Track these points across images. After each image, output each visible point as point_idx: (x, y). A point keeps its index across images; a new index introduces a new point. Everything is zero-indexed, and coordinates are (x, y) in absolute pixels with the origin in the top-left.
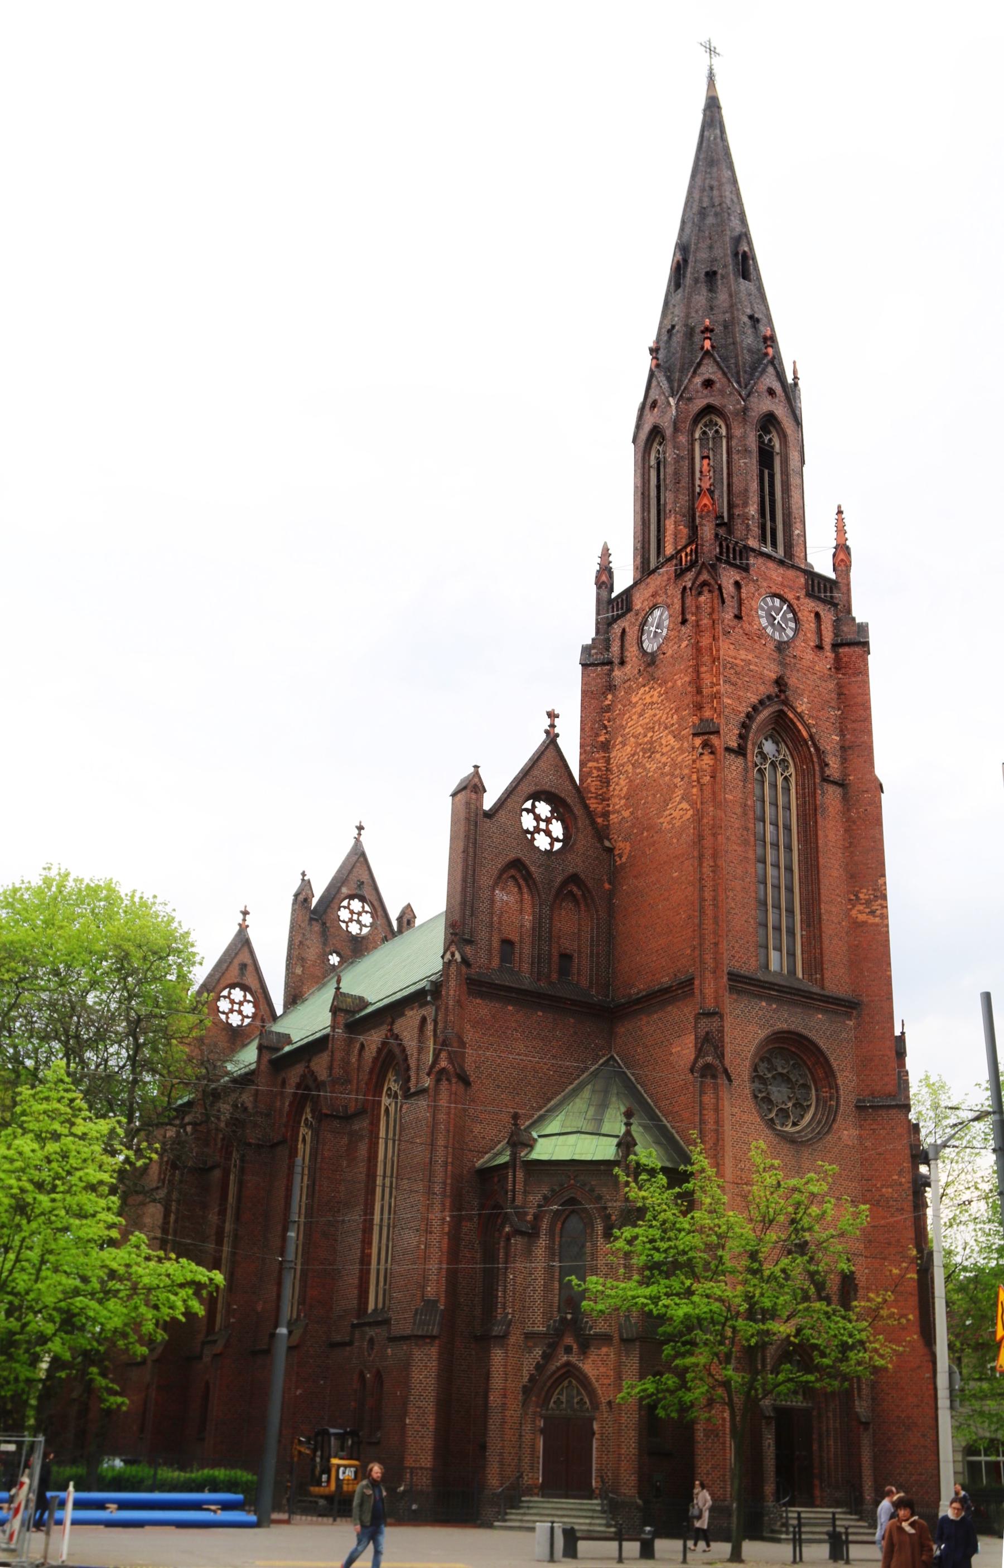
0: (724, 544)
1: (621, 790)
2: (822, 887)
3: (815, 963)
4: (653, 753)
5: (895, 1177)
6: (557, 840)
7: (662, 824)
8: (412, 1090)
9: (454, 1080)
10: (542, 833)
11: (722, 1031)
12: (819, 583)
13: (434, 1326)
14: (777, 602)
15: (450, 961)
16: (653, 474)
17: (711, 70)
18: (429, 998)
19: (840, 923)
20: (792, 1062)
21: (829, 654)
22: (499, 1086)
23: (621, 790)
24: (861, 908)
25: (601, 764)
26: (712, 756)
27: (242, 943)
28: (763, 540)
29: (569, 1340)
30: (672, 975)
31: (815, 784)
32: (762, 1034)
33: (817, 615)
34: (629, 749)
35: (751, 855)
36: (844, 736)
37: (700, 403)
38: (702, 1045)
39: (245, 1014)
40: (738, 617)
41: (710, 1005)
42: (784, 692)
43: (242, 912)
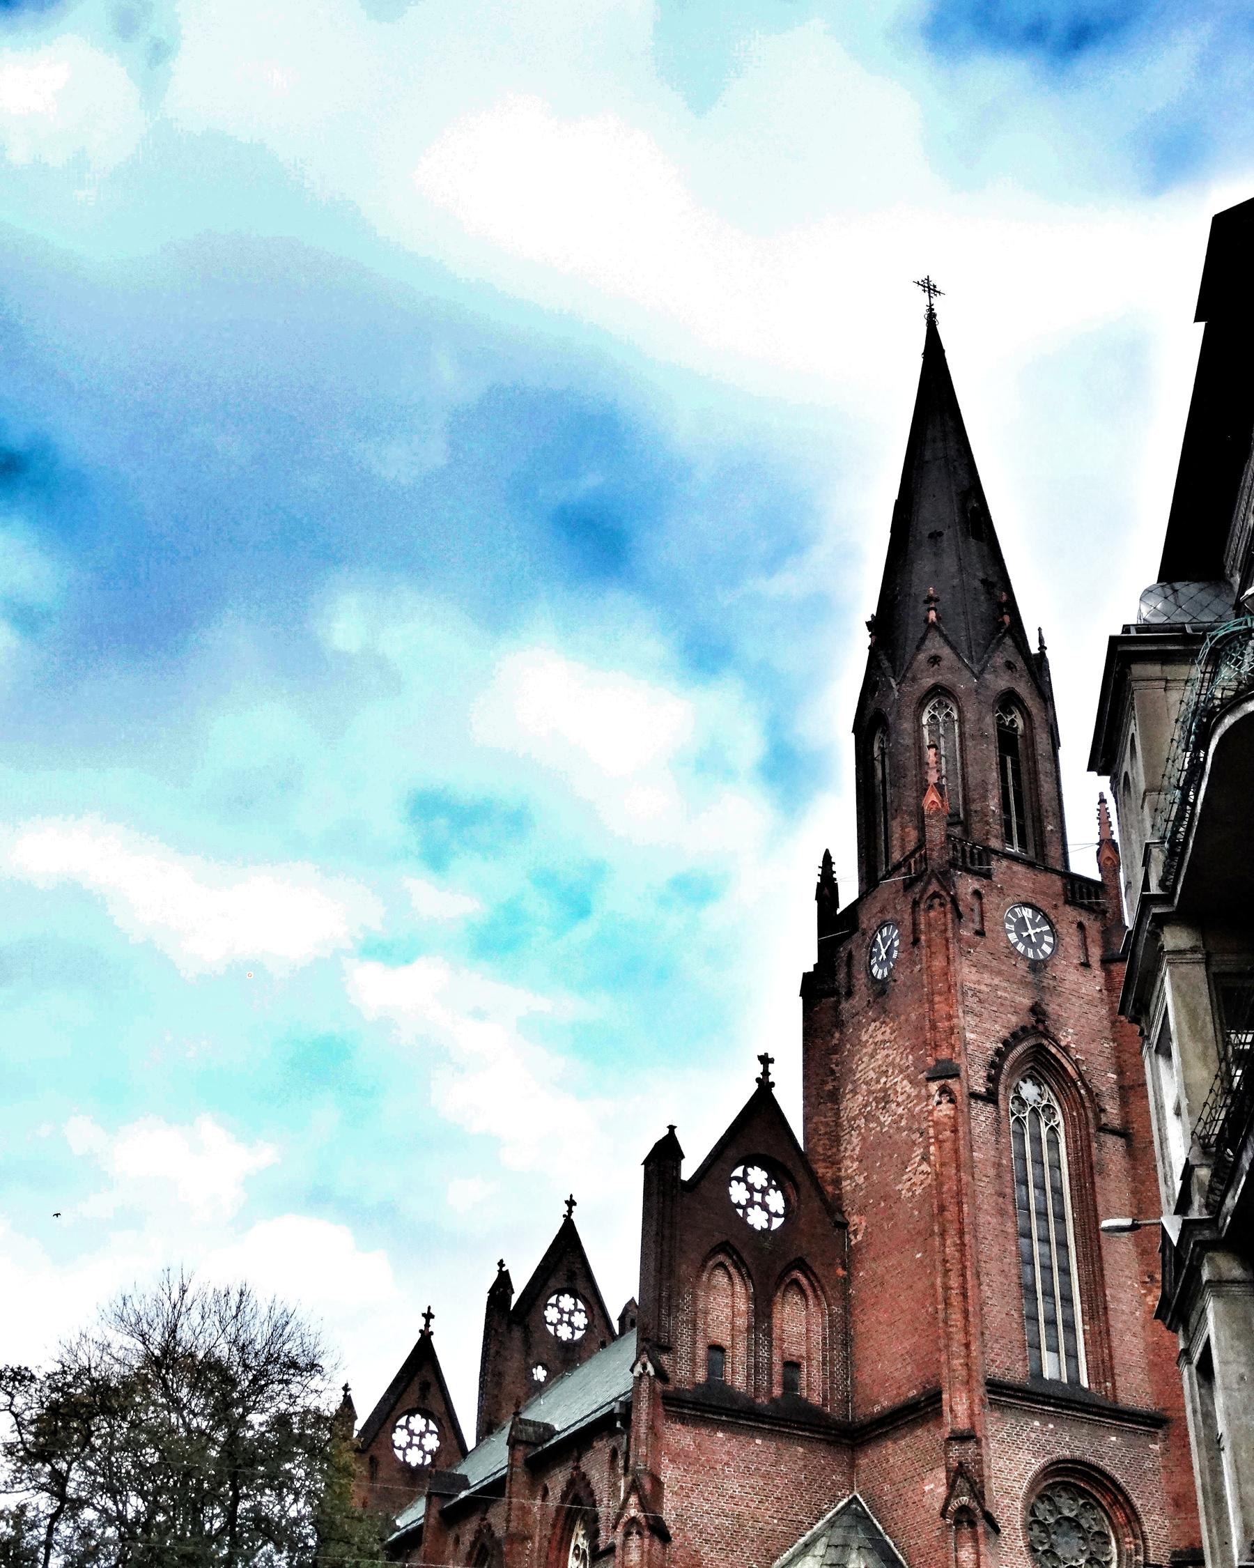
1: (854, 1150)
2: (1106, 1266)
3: (1104, 1368)
4: (887, 1103)
6: (777, 1215)
8: (602, 1547)
9: (647, 1533)
10: (757, 1207)
11: (980, 1462)
12: (1081, 888)
15: (641, 1375)
17: (931, 309)
18: (618, 1425)
20: (1081, 1502)
21: (1098, 971)
22: (707, 1541)
26: (951, 1106)
27: (423, 1358)
28: (1008, 838)
30: (920, 1387)
31: (1088, 1134)
32: (1037, 1464)
33: (1081, 926)
34: (861, 1098)
35: (1010, 1229)
37: (928, 682)
39: (427, 1449)
40: (980, 933)
41: (963, 1424)
42: (1043, 1022)
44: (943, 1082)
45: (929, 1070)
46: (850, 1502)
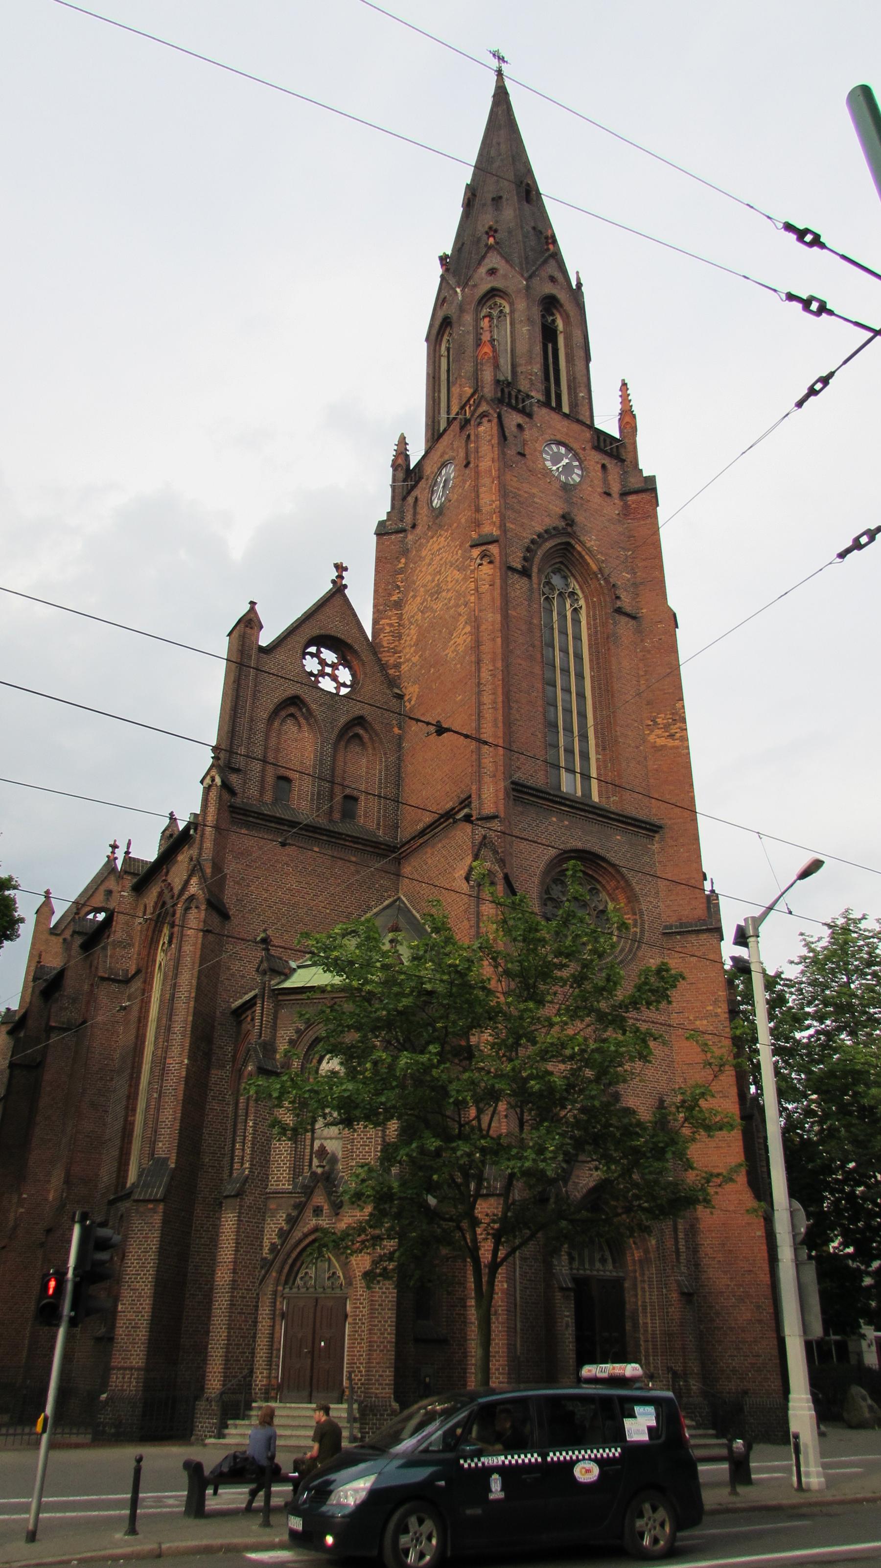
0: (506, 390)
1: (412, 639)
5: (710, 1008)
6: (344, 685)
7: (446, 655)
13: (159, 1187)
14: (563, 450)
15: (210, 786)
16: (444, 361)
19: (637, 747)
23: (412, 639)
24: (659, 732)
25: (394, 620)
26: (491, 566)
29: (319, 1199)
33: (604, 467)
36: (635, 573)
37: (484, 287)
38: (479, 850)
43: (111, 846)
44: (484, 548)
45: (472, 541)
46: (395, 901)
